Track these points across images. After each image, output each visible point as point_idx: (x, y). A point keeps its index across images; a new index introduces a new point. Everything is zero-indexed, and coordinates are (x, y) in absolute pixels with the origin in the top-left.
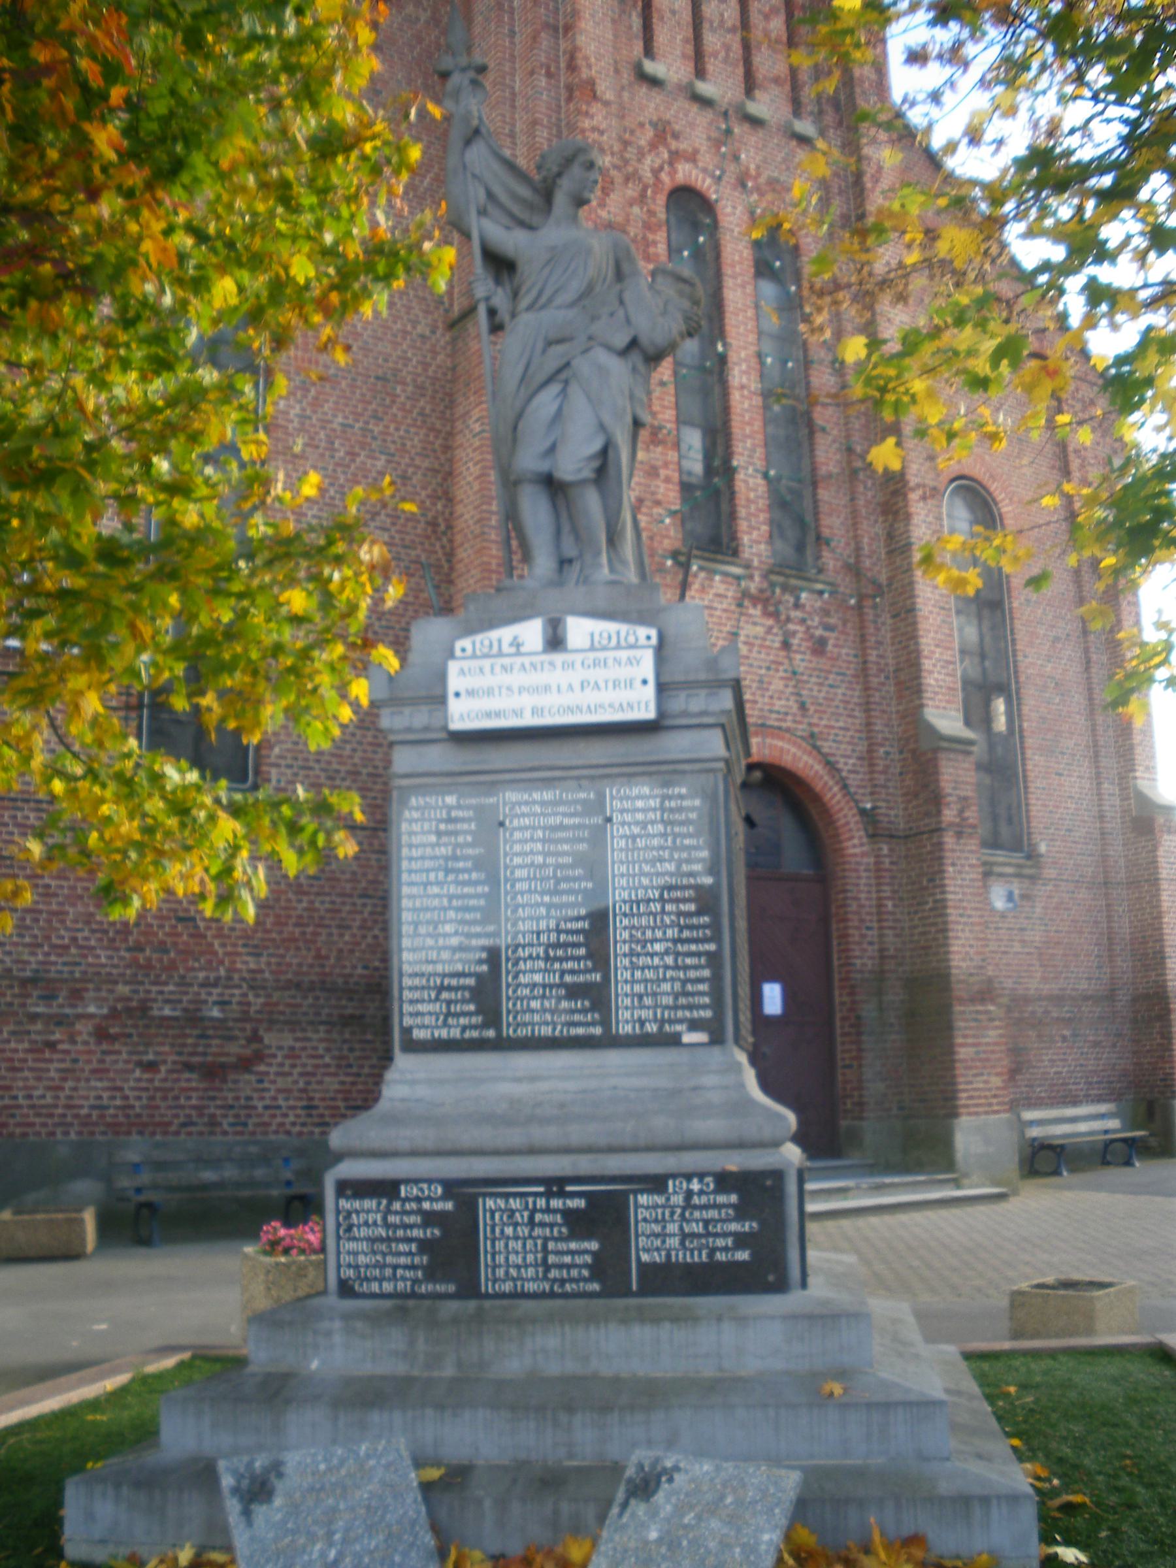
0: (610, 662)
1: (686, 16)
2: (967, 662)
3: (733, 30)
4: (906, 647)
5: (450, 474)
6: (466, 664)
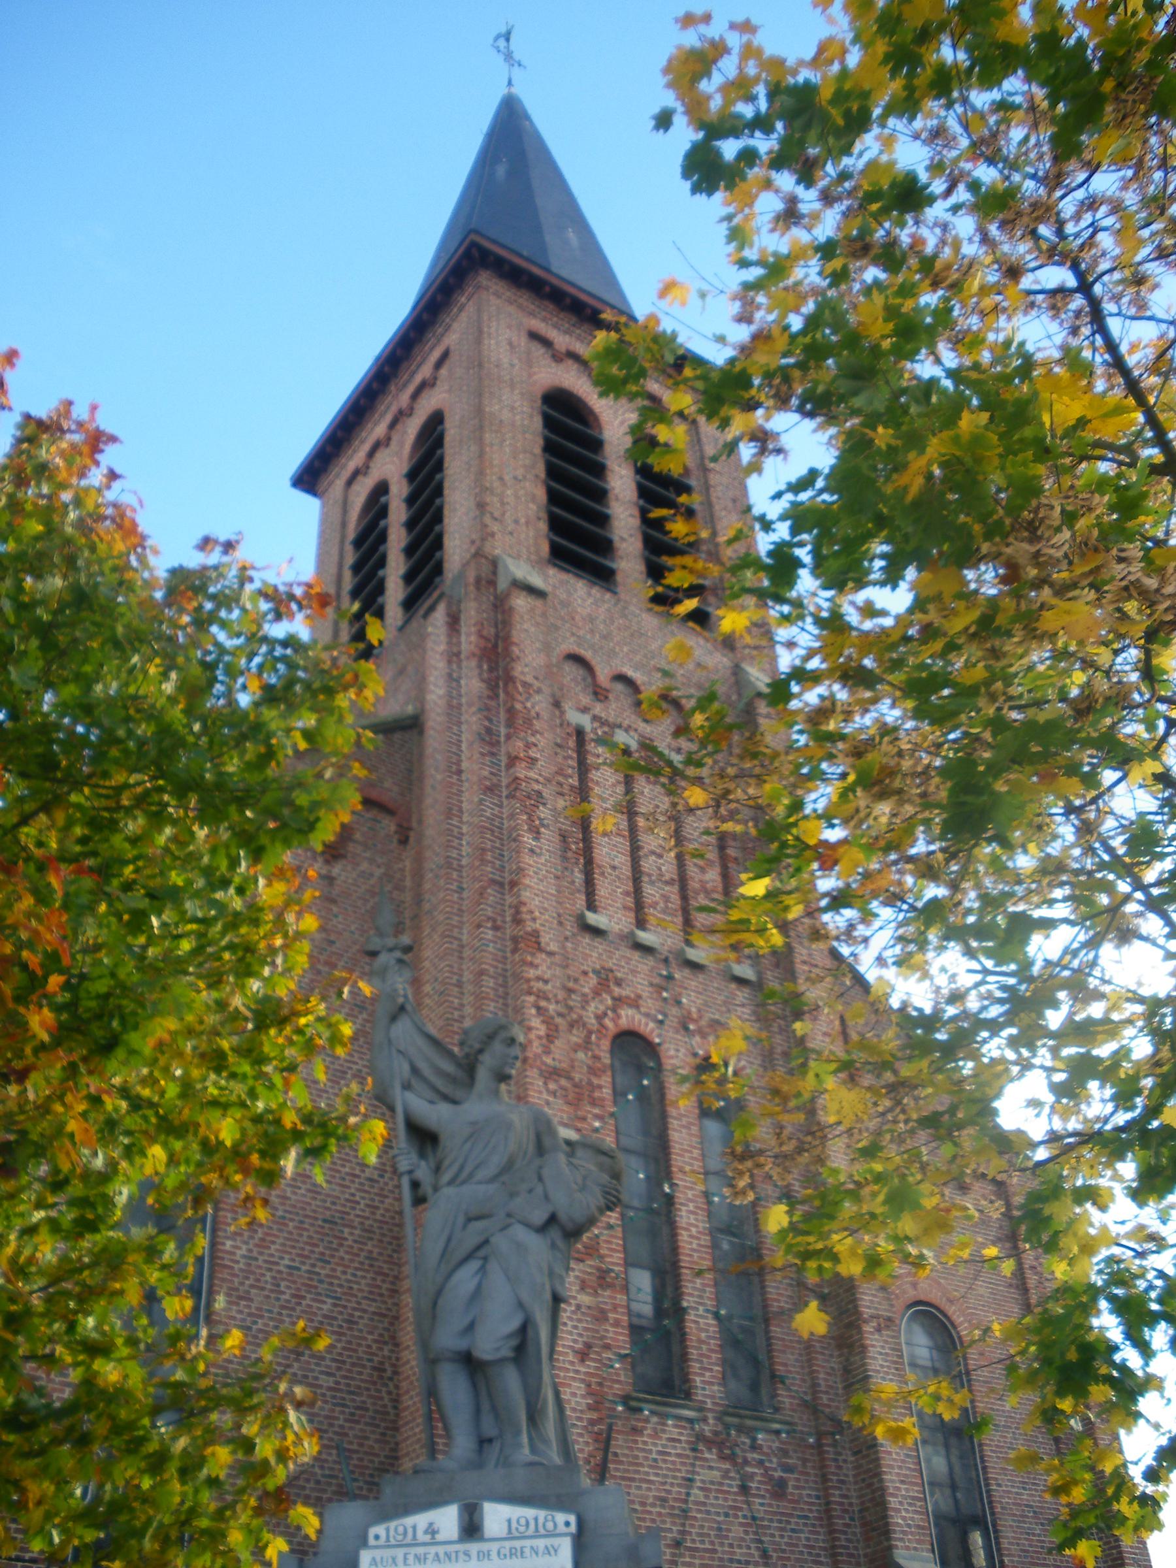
0: (527, 1551)
1: (626, 871)
2: (937, 1495)
3: (670, 882)
4: (870, 1485)
5: (396, 1318)
6: (378, 1553)
